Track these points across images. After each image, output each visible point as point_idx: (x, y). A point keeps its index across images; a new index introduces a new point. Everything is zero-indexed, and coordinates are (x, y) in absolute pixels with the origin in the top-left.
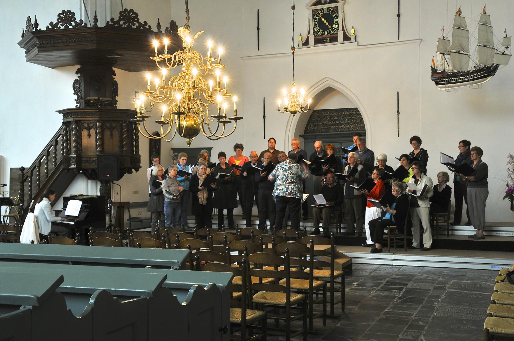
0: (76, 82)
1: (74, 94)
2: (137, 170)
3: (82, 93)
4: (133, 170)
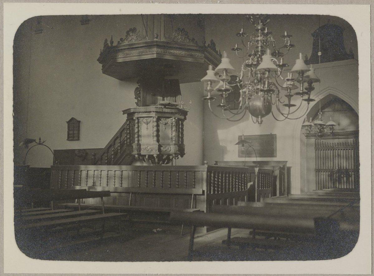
0: (137, 89)
1: (135, 98)
2: (182, 156)
3: (141, 97)
4: (179, 156)
